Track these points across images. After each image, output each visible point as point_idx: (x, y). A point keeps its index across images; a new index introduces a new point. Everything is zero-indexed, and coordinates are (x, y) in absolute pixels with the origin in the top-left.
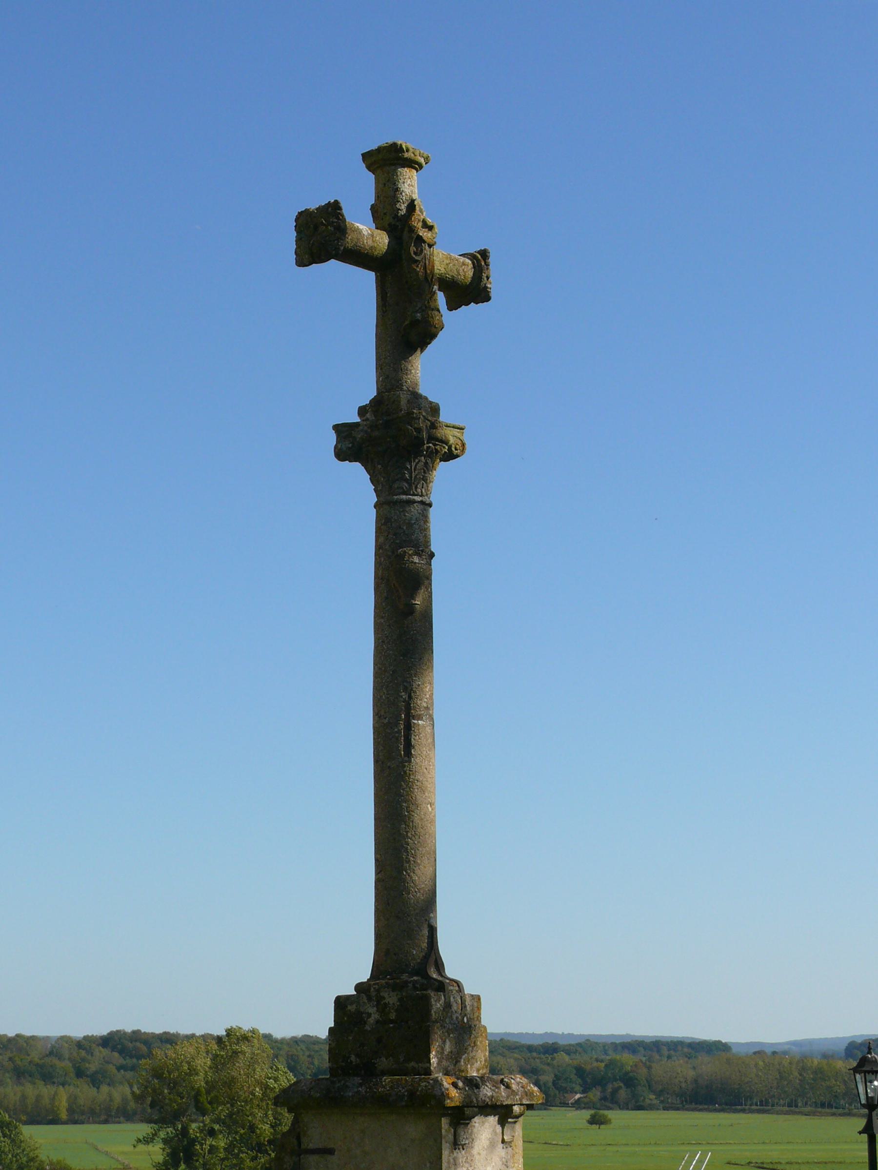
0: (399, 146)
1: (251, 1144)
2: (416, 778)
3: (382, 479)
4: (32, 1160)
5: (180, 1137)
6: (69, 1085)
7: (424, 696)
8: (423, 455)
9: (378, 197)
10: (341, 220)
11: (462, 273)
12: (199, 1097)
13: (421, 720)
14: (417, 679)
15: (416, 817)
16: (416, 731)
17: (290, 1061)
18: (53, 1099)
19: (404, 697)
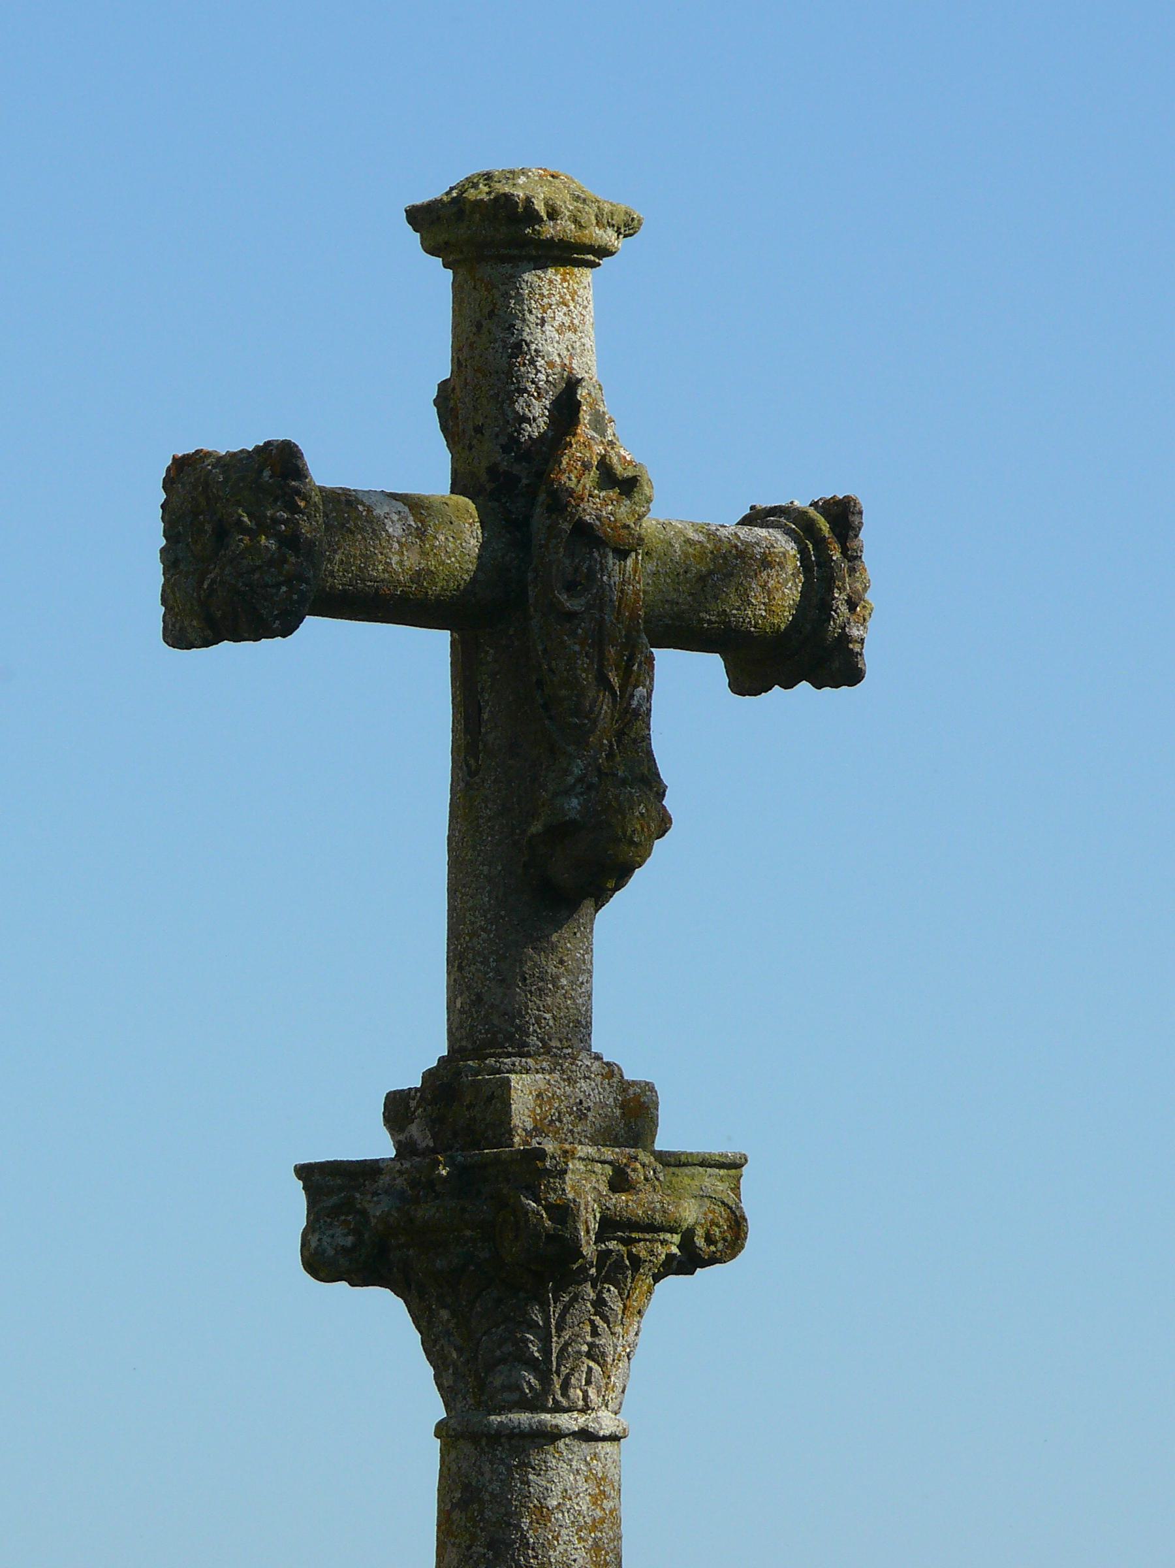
3: (455, 1355)
10: (301, 512)
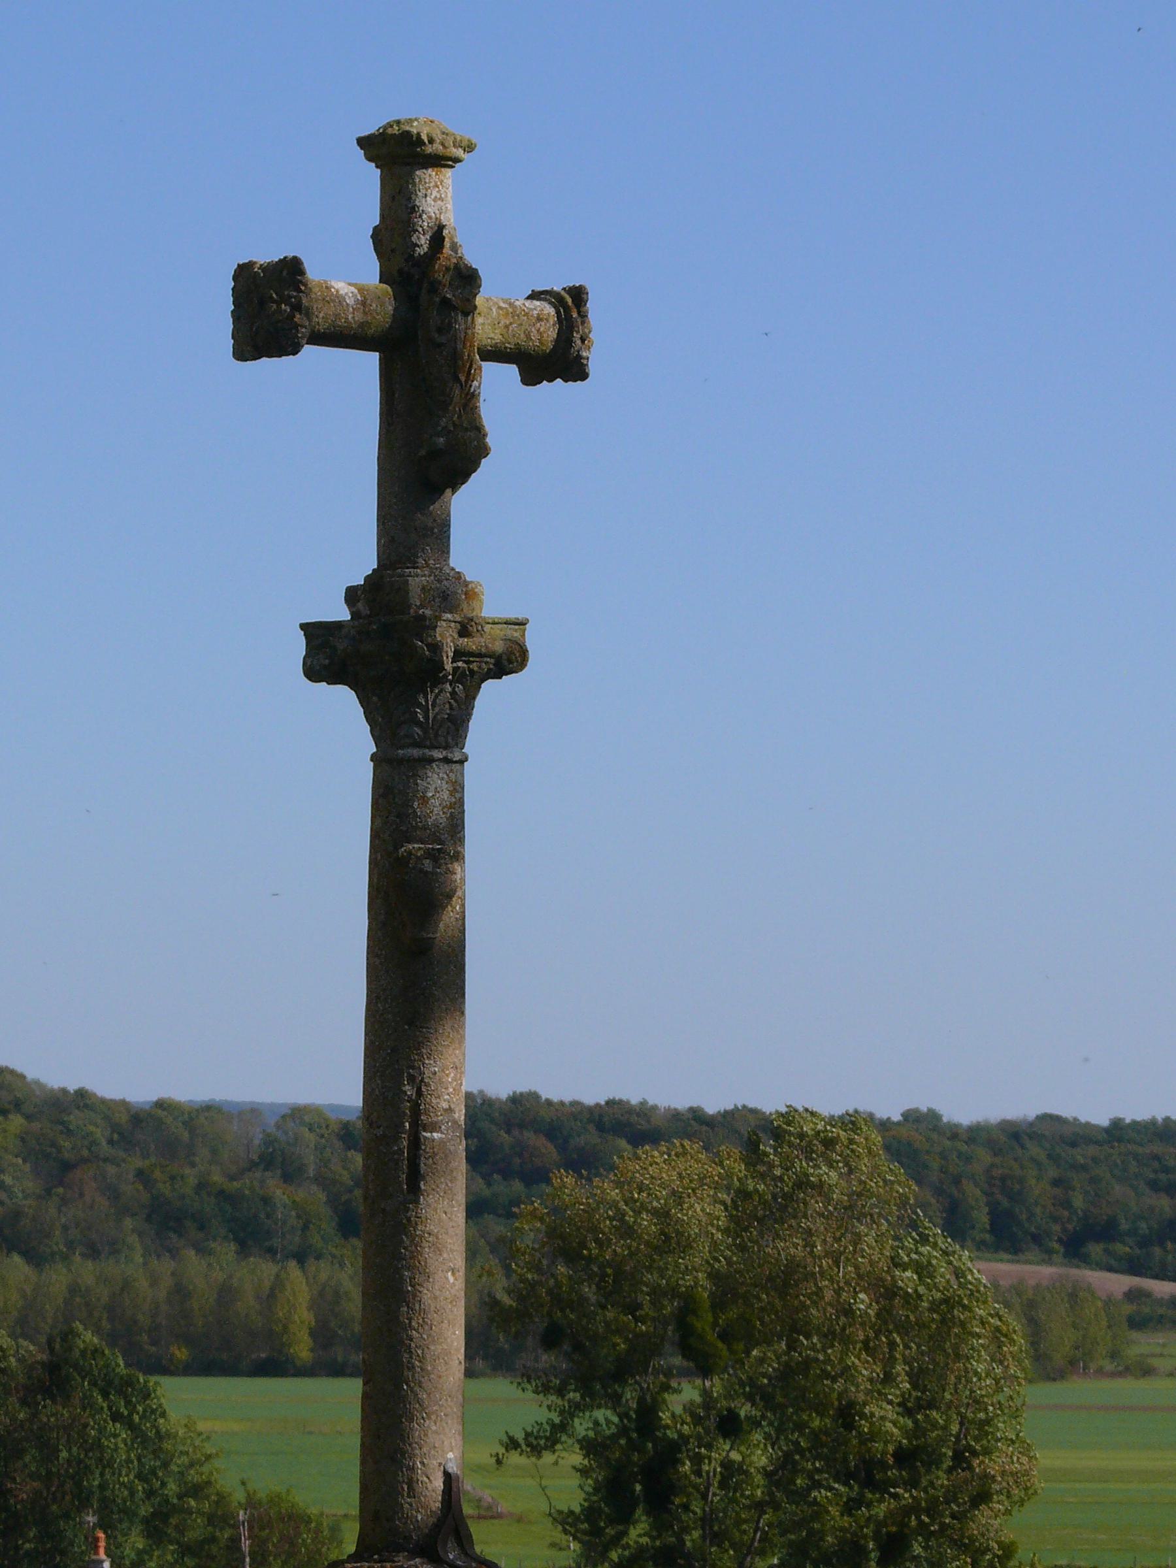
0: (415, 137)
1: (845, 1460)
2: (428, 1229)
3: (380, 719)
4: (196, 1491)
5: (635, 1435)
6: (318, 1257)
7: (443, 1090)
9: (382, 216)
10: (302, 292)
11: (534, 336)
12: (691, 1319)
13: (438, 1132)
14: (432, 1062)
15: (426, 1294)
16: (428, 1150)
17: (999, 1197)
18: (271, 1297)
19: (409, 1093)
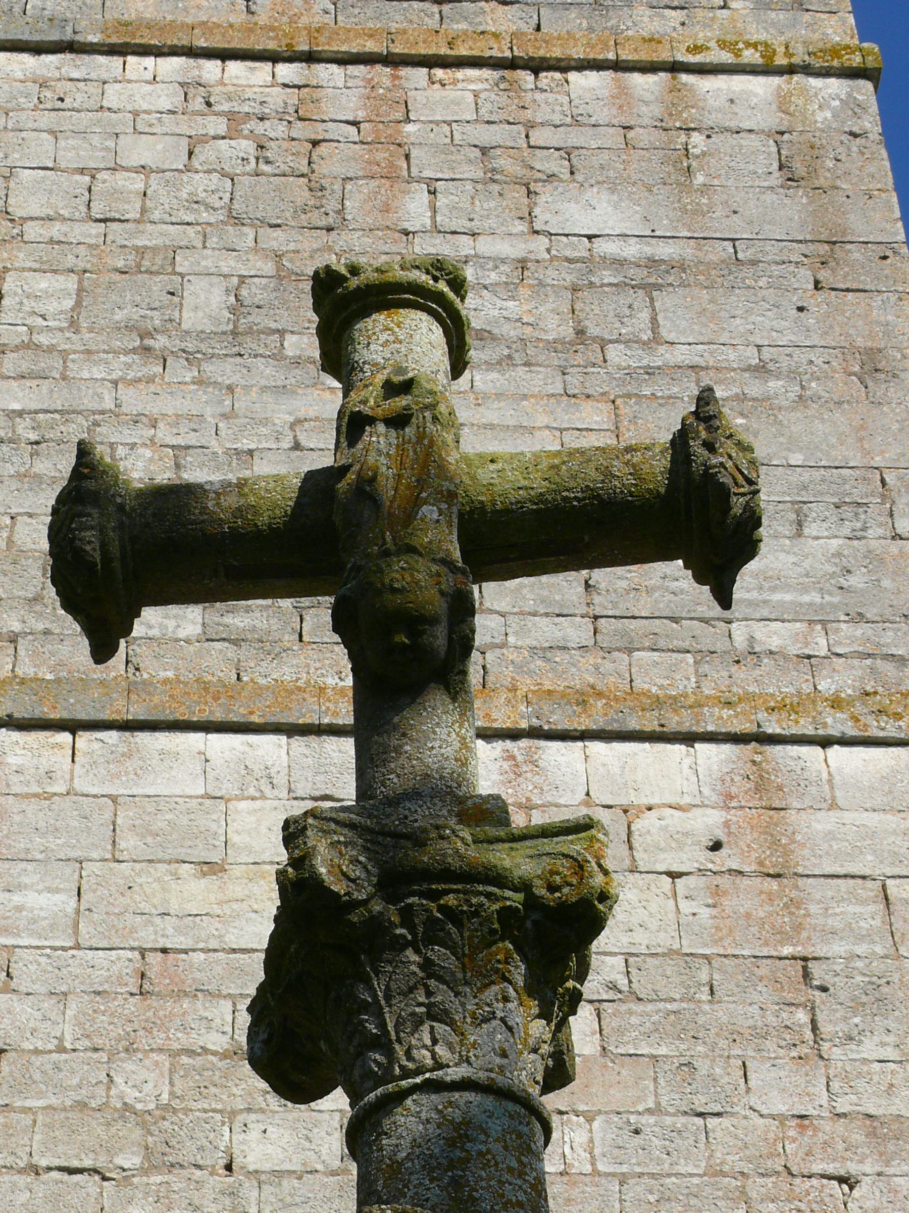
8: (400, 945)
